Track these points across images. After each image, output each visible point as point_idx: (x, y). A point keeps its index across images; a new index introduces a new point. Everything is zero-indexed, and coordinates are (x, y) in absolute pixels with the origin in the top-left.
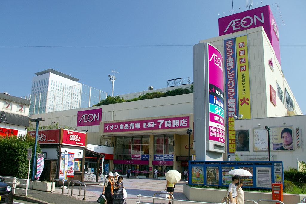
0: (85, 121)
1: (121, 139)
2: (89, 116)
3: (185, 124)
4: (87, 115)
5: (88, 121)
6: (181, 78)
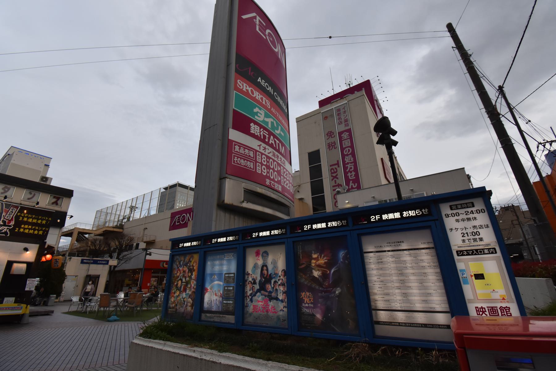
0: (177, 223)
1: (214, 360)
2: (182, 217)
3: (413, 212)
4: (180, 216)
5: (180, 223)
6: (551, 127)
